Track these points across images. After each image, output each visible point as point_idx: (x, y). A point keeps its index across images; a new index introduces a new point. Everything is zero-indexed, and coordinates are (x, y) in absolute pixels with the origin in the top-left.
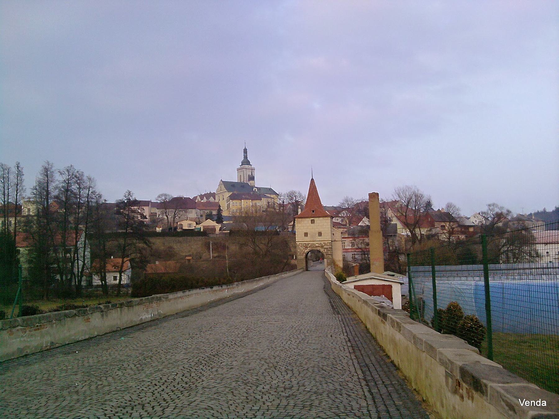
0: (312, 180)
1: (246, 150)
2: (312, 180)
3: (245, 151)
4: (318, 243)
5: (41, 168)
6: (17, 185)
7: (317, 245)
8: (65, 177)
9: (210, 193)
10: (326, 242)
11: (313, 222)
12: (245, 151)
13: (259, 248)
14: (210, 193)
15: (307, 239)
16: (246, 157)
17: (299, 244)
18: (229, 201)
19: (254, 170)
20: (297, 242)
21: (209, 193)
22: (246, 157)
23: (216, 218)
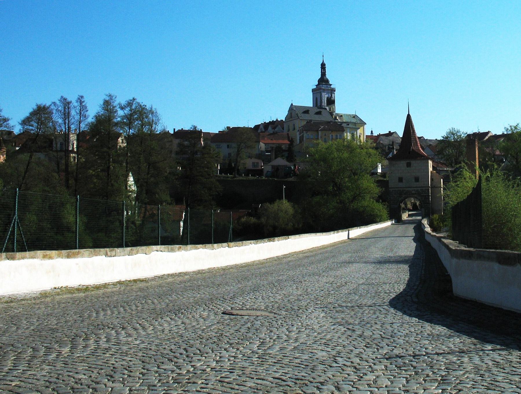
0: (409, 117)
1: (325, 65)
2: (409, 117)
3: (323, 66)
4: (414, 190)
5: (102, 102)
6: (80, 123)
7: (413, 192)
8: (127, 111)
9: (277, 120)
10: (424, 188)
11: (409, 165)
12: (323, 66)
13: (80, 117)
14: (277, 120)
15: (401, 185)
16: (323, 74)
17: (392, 190)
18: (303, 132)
19: (335, 91)
20: (390, 188)
21: (275, 120)
22: (323, 74)
23: (286, 154)
